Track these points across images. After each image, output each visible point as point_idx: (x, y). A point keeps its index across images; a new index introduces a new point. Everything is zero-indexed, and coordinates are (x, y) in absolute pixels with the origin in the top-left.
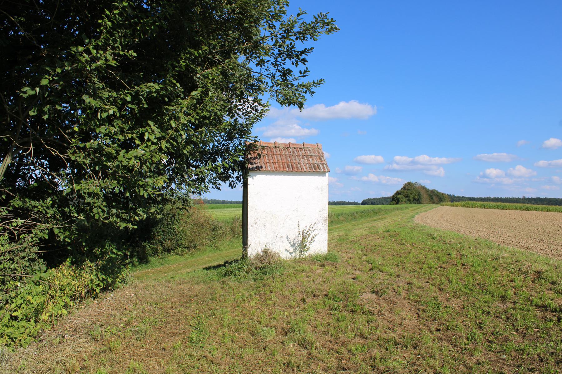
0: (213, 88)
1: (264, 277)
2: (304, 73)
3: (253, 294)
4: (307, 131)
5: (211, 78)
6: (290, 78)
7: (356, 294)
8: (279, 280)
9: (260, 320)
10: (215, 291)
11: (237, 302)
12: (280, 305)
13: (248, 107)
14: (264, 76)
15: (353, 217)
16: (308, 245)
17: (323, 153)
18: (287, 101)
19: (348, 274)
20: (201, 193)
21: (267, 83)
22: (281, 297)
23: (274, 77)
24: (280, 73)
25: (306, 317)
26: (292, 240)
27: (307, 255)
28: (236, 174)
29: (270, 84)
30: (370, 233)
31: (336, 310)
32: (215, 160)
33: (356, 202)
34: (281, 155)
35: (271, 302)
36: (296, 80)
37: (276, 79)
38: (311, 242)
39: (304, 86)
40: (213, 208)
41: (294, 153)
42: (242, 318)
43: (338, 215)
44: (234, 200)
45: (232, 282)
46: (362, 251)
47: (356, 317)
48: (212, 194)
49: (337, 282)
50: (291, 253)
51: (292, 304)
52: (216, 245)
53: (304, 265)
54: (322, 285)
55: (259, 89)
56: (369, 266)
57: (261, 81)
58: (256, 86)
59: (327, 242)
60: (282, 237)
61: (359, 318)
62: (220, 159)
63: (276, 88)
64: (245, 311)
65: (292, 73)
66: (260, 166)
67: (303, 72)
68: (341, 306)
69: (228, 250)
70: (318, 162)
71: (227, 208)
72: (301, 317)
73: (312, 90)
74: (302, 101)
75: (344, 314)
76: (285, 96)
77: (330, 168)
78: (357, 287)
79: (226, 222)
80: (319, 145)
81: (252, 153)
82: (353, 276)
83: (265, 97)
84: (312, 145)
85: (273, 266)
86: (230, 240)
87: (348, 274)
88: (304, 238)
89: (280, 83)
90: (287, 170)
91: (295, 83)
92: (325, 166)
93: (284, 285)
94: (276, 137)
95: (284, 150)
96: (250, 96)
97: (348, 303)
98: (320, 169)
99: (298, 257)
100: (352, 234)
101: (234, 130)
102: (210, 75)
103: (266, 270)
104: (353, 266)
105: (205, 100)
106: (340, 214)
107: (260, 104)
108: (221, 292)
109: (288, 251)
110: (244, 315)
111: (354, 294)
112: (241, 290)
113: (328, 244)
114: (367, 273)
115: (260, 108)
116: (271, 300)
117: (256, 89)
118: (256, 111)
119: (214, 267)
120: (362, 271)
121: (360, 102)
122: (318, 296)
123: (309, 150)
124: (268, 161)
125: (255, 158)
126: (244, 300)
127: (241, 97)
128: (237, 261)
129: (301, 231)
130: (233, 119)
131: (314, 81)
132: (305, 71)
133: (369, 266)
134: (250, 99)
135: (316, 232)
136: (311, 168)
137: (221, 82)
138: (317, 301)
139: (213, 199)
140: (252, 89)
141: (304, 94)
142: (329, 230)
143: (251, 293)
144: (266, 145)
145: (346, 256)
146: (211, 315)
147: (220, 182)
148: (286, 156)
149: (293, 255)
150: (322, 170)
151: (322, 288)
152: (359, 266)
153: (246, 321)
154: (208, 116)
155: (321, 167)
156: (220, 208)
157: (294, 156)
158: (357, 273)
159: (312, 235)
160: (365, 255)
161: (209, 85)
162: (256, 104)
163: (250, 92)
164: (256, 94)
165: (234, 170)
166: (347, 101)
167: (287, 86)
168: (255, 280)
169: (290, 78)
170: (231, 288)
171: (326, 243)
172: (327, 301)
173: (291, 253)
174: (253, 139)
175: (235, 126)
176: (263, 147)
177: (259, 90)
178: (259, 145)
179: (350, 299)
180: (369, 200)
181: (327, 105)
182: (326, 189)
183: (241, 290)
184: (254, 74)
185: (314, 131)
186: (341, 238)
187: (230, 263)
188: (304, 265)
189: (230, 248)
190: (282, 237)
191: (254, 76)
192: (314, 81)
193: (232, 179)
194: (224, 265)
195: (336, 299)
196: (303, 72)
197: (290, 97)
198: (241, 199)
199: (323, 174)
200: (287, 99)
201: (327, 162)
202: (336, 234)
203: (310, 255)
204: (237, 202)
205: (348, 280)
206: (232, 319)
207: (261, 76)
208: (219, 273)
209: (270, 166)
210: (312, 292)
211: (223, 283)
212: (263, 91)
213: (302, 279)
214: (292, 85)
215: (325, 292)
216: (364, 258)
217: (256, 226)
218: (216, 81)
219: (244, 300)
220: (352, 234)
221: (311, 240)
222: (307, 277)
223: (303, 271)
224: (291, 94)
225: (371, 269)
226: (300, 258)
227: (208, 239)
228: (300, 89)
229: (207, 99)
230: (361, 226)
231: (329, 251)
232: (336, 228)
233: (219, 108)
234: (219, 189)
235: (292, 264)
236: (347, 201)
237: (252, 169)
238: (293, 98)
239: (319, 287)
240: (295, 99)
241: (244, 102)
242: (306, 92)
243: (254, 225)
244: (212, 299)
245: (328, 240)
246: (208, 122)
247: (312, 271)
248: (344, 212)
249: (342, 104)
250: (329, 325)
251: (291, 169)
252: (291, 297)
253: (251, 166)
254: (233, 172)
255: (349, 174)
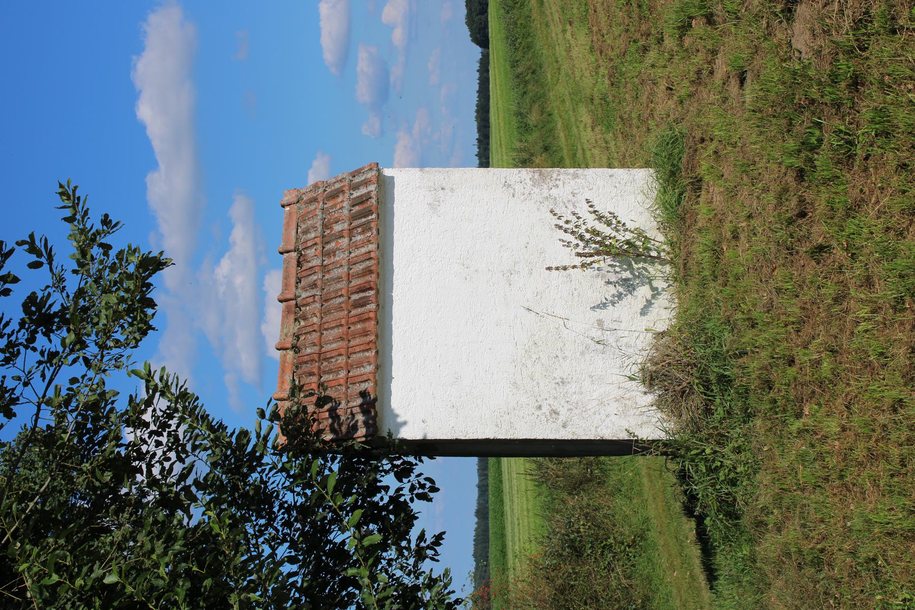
0: (91, 570)
1: (737, 383)
2: (40, 253)
3: (797, 424)
4: (239, 234)
5: (55, 578)
6: (57, 302)
7: (795, 73)
8: (749, 334)
9: (888, 401)
10: (788, 555)
11: (826, 479)
12: (834, 331)
13: (158, 444)
14: (51, 393)
15: (529, 78)
16: (629, 236)
17: (316, 186)
18: (138, 312)
19: (725, 100)
20: (453, 597)
21: (74, 381)
22: (807, 330)
23: (53, 355)
24: (39, 336)
25: (877, 244)
26: (612, 290)
27: (661, 238)
28: (390, 480)
29: (79, 369)
30: (584, 19)
31: (851, 143)
32: (340, 552)
33: (477, 66)
34: (321, 329)
35: (826, 365)
36: (62, 279)
37: (60, 349)
38: (619, 226)
39: (84, 253)
40: (503, 552)
41: (314, 285)
42: (882, 464)
43: (524, 128)
44: (475, 479)
45: (761, 493)
46: (645, 49)
47: (876, 73)
48: (456, 564)
49: (754, 138)
50: (656, 292)
51: (830, 290)
52: (629, 540)
53: (696, 248)
54: (766, 190)
55: (94, 406)
56: (699, 26)
57: (67, 402)
58: (85, 418)
59: (620, 172)
60: (600, 323)
61: (882, 63)
62: (337, 537)
63: (92, 350)
64: (860, 453)
65: (40, 295)
66: (359, 401)
67: (33, 258)
68: (837, 123)
69: (649, 501)
70: (344, 201)
71: (502, 501)
72: (878, 261)
73: (98, 226)
74: (135, 259)
75: (866, 114)
76: (117, 316)
77: (365, 164)
78: (770, 68)
79: (550, 509)
80: (285, 200)
81: (315, 427)
82: (734, 83)
83: (123, 387)
84: (288, 224)
85: (701, 352)
86: (612, 494)
87: (725, 100)
88: (605, 249)
89: (72, 337)
90: (372, 306)
91: (73, 283)
92: (357, 180)
93: (766, 318)
94: (260, 341)
95: (305, 319)
96: (118, 438)
97: (827, 99)
98: (368, 197)
99: (668, 268)
100: (588, 82)
101: (235, 488)
102: (46, 581)
103: (713, 378)
104: (698, 81)
105: (131, 596)
106: (521, 127)
107: (149, 403)
108: (792, 532)
109: (649, 304)
110: (872, 456)
111: (797, 78)
112: (783, 464)
113: (623, 165)
114: (724, 33)
115: (162, 404)
116: (818, 362)
117: (96, 419)
118: (170, 417)
119: (707, 551)
120: (714, 52)
121: (139, 49)
122: (802, 201)
123: (306, 232)
124: (342, 374)
125: (333, 413)
126: (820, 457)
127: (123, 468)
128: (683, 476)
129: (578, 261)
130: (199, 495)
131: (66, 219)
132: (33, 249)
133: (699, 26)
134: (129, 435)
135: (583, 210)
136: (366, 228)
137: (68, 540)
138: (821, 207)
139: (471, 549)
140: (96, 431)
141: (113, 253)
142: (576, 165)
143: (794, 428)
144: (288, 377)
145: (665, 105)
146: (877, 572)
147: (414, 534)
148: (325, 313)
149: (660, 284)
150: (372, 188)
151: (775, 188)
152: (698, 59)
153: (895, 452)
154: (188, 584)
155: (363, 191)
156: (503, 528)
157: (325, 283)
158: (722, 67)
159: (592, 222)
160: (660, 41)
161: (79, 582)
162: (147, 417)
163: (105, 438)
164: (113, 418)
165: (374, 488)
166: (132, 95)
167: (85, 310)
168: (748, 415)
169: (57, 302)
170: (778, 500)
171: (620, 173)
172: (822, 173)
173: (656, 292)
174: (266, 424)
175: (221, 488)
176: (296, 389)
177: (98, 408)
178: (287, 404)
179: (814, 92)
180: (470, 21)
181: (153, 165)
182: (436, 175)
183: (783, 464)
184: (42, 425)
185: (239, 209)
186: (603, 120)
187: (693, 498)
188: (692, 247)
189: (640, 494)
190: (600, 323)
191: (48, 427)
192: (66, 219)
193: (406, 491)
194: (700, 520)
195: (813, 140)
196: (33, 258)
197: (122, 300)
198: (472, 462)
199: (385, 185)
200: (129, 311)
201: (344, 171)
202: (588, 136)
203: (663, 227)
204: (483, 471)
205: (748, 98)
206: (886, 500)
207: (49, 403)
208: (726, 538)
209: (360, 365)
210: (790, 222)
211: (760, 524)
212: (103, 394)
213: (744, 257)
214: (81, 293)
215: (790, 179)
216: (670, 43)
217: (563, 412)
218: (64, 558)
219: (820, 457)
220: (588, 82)
221: (609, 224)
222: (736, 237)
223: (717, 253)
224: (113, 299)
225: (710, 20)
226: (671, 262)
227: (610, 568)
228: (94, 268)
229: (129, 589)
230: (560, 51)
231: (647, 165)
232: (568, 136)
233: (159, 546)
234: (438, 539)
235: (693, 288)
236: (474, 99)
237: (372, 424)
238: (127, 290)
239: (771, 197)
240: (130, 284)
241: (141, 456)
242: (107, 248)
243: (562, 418)
244: (817, 563)
245: (610, 166)
246: (208, 582)
247: (718, 220)
248: (514, 108)
249: (145, 112)
250: (904, 166)
251: (365, 300)
252: (808, 295)
253: (362, 431)
254: (379, 490)
255: (383, 90)
